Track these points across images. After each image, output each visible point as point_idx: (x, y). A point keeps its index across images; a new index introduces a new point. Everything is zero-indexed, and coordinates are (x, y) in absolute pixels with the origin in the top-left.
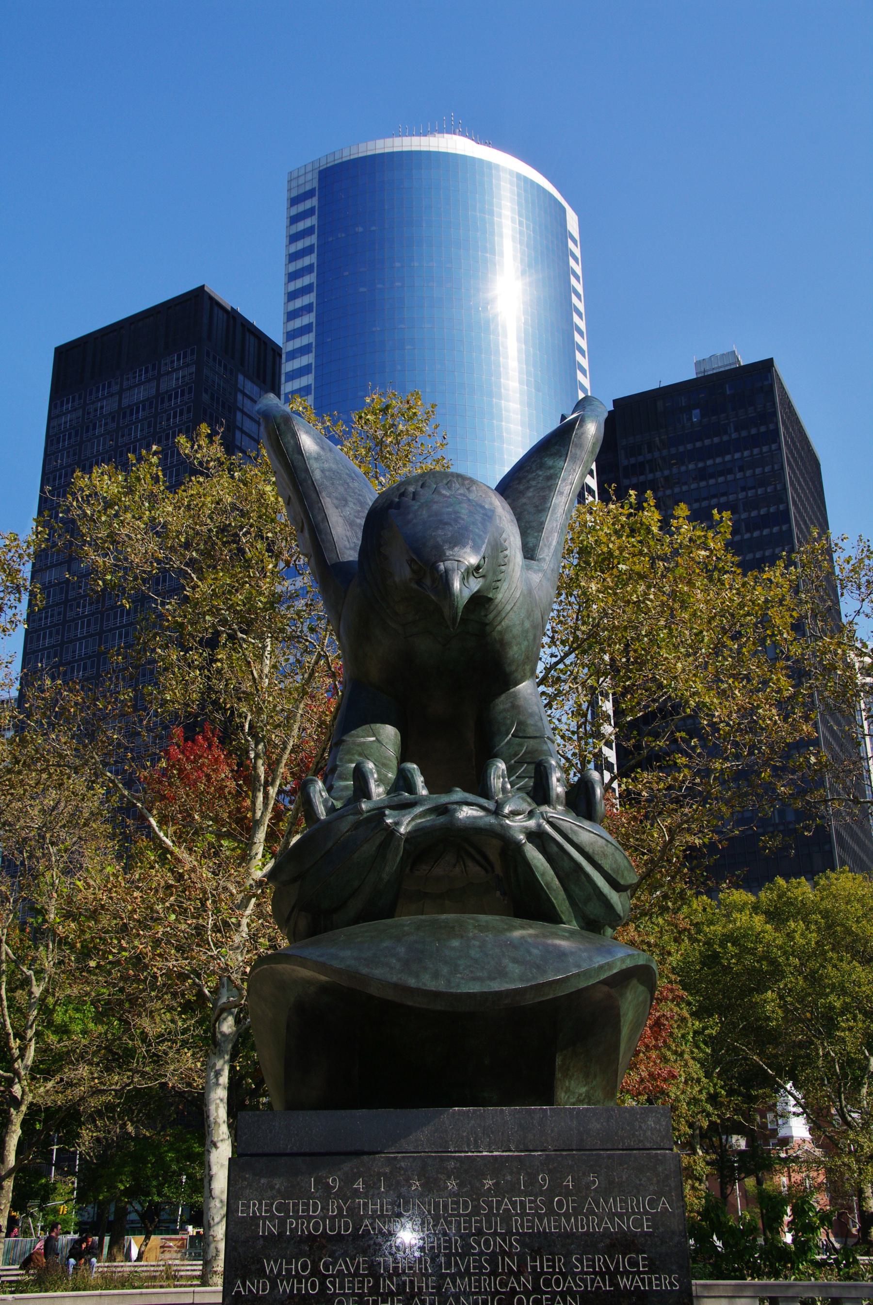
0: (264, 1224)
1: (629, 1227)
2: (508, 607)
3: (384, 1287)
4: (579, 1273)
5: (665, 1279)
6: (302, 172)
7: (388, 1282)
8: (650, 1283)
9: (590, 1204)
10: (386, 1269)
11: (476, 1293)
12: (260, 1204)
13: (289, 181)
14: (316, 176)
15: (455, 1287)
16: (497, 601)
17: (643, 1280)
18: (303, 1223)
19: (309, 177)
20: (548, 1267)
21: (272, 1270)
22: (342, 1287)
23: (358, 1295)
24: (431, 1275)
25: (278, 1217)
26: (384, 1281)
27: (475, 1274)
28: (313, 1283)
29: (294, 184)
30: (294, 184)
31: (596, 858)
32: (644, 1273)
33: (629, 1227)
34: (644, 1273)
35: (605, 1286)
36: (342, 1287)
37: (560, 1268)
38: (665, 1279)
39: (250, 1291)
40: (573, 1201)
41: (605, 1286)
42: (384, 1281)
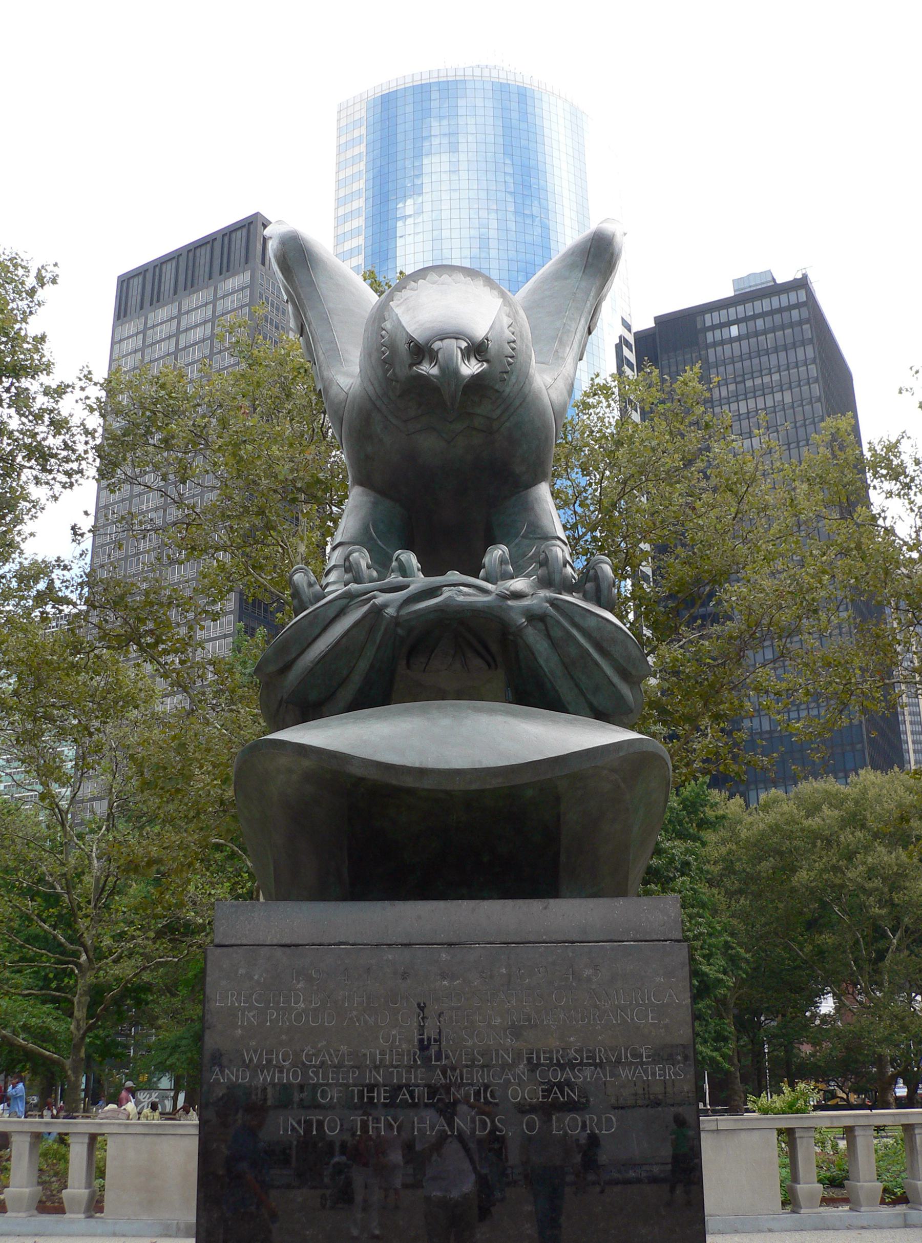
0: (243, 1014)
1: (632, 1019)
2: (517, 403)
3: (370, 1078)
4: (578, 1064)
5: (670, 1069)
6: (351, 103)
7: (374, 1073)
8: (654, 1074)
9: (556, 1093)
10: (373, 1060)
11: (469, 1084)
12: (239, 994)
13: (339, 112)
14: (364, 105)
15: (445, 1078)
16: (506, 393)
17: (645, 1071)
18: (284, 1015)
19: (357, 107)
20: (545, 1059)
21: (251, 1060)
22: (325, 1077)
23: (341, 1085)
24: (419, 1067)
25: (257, 1008)
26: (371, 1072)
27: (467, 1066)
28: (295, 1073)
29: (343, 114)
30: (343, 114)
31: (605, 645)
32: (648, 1063)
33: (632, 1019)
34: (648, 1063)
35: (605, 1076)
36: (325, 1077)
37: (558, 1060)
38: (670, 1069)
39: (229, 1079)
40: (385, 1091)
41: (605, 1076)
42: (371, 1072)
